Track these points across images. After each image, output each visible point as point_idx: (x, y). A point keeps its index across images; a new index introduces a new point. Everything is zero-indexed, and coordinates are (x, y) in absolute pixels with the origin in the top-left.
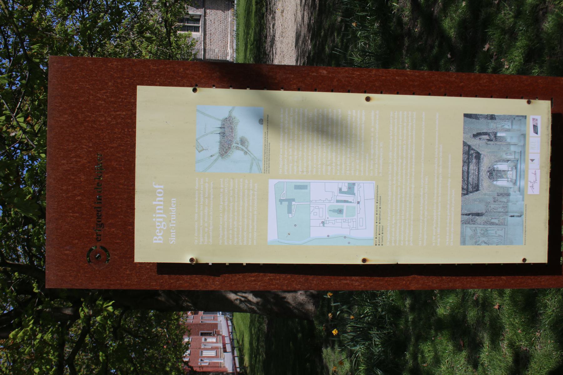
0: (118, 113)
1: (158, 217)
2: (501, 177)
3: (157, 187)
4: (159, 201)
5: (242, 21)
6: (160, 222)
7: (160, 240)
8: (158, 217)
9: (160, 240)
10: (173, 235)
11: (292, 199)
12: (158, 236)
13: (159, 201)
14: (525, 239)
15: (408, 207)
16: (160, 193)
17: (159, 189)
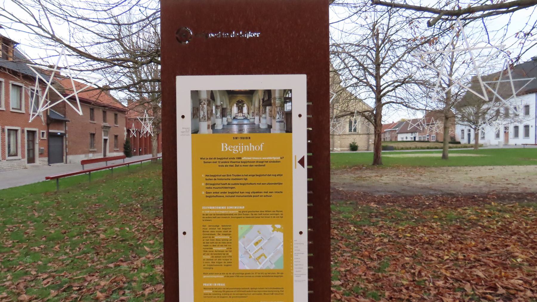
0: (289, 47)
1: (241, 148)
2: (239, 109)
3: (261, 146)
4: (252, 147)
5: (85, 100)
6: (238, 149)
7: (225, 149)
8: (241, 148)
9: (225, 149)
10: (247, 148)
11: (291, 128)
12: (228, 147)
13: (252, 147)
14: (256, 193)
15: (218, 284)
16: (257, 148)
17: (260, 147)
